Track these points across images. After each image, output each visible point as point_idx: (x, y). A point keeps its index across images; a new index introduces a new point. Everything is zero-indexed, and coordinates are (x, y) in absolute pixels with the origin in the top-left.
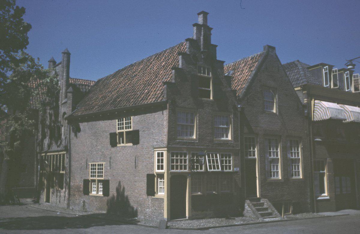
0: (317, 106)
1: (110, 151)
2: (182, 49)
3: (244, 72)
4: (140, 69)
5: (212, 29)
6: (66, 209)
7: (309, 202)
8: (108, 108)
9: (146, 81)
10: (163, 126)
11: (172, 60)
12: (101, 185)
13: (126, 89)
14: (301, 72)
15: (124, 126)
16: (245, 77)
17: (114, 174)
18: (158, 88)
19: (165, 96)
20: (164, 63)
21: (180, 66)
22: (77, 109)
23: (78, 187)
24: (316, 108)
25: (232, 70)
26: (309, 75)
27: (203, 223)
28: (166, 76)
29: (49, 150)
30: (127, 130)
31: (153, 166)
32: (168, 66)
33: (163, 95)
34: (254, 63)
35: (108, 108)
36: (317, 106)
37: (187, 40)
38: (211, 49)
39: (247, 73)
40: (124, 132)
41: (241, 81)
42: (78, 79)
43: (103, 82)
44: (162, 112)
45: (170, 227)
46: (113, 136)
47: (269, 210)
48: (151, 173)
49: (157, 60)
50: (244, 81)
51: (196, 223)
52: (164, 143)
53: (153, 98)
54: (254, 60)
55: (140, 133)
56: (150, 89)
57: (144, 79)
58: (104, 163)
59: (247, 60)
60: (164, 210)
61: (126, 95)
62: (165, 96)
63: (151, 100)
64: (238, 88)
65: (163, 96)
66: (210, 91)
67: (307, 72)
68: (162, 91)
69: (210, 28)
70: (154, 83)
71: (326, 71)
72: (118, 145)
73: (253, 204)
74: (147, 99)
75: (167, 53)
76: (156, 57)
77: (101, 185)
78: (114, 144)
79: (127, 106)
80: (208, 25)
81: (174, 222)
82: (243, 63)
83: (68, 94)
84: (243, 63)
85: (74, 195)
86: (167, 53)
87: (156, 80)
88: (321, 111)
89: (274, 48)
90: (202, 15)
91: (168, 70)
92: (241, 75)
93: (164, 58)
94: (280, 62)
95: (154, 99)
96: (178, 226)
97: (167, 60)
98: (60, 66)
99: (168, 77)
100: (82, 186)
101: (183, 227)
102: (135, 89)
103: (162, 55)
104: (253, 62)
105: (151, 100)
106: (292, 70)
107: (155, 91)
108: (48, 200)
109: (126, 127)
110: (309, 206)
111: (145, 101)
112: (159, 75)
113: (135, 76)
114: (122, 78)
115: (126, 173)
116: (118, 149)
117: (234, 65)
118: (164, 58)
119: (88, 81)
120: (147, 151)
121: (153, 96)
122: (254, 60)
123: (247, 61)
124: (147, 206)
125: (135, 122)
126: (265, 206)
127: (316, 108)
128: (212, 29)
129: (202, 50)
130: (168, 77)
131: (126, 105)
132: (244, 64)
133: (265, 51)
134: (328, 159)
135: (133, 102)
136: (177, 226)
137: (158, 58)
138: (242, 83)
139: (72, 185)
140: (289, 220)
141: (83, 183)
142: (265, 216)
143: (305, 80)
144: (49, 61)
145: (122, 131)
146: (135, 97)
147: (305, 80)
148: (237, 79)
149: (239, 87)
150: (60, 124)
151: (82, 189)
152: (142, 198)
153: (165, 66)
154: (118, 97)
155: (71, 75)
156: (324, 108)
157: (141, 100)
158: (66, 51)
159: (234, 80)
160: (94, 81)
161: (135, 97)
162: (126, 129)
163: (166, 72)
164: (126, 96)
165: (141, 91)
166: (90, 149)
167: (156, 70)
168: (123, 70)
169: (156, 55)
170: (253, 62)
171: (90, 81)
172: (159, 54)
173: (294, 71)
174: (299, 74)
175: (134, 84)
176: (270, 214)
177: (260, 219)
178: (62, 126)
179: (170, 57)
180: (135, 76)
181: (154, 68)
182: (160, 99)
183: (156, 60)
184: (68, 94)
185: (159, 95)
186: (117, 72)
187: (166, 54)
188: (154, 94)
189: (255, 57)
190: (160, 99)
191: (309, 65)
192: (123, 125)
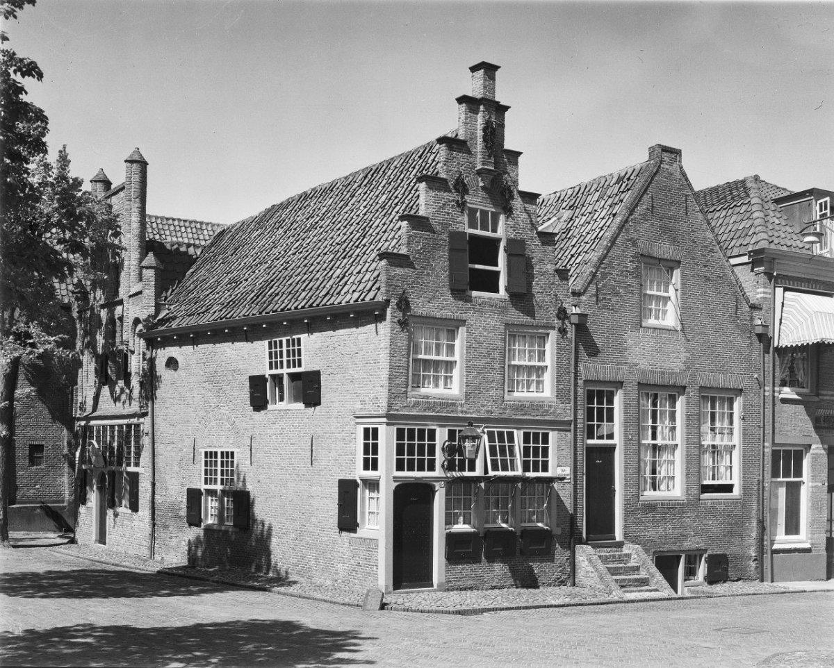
0: (791, 306)
1: (251, 422)
2: (430, 162)
3: (595, 218)
4: (325, 209)
5: (507, 108)
6: (146, 561)
7: (753, 554)
8: (241, 312)
9: (338, 244)
10: (378, 363)
11: (405, 191)
12: (230, 502)
13: (288, 263)
14: (756, 215)
15: (285, 359)
16: (598, 230)
17: (261, 478)
18: (367, 265)
19: (383, 289)
20: (385, 196)
21: (422, 213)
22: (168, 312)
23: (173, 509)
24: (789, 313)
25: (568, 208)
26: (777, 222)
27: (472, 599)
28: (386, 234)
29: (95, 414)
30: (292, 370)
31: (353, 461)
32: (393, 206)
33: (377, 286)
34: (623, 192)
35: (243, 312)
36: (791, 306)
37: (441, 140)
38: (503, 160)
39: (604, 221)
40: (285, 375)
41: (587, 243)
42: (168, 219)
43: (233, 237)
44: (374, 325)
45: (390, 607)
46: (257, 384)
47: (642, 573)
48: (349, 477)
49: (368, 185)
50: (594, 242)
51: (454, 599)
52: (379, 406)
53: (354, 291)
54: (624, 185)
55: (323, 378)
56: (348, 267)
57: (335, 237)
58: (236, 450)
59: (607, 183)
60: (379, 567)
61: (287, 278)
62: (383, 289)
63: (349, 296)
64: (577, 261)
65: (379, 289)
66: (498, 273)
67: (772, 214)
68: (376, 273)
69: (501, 105)
70: (359, 250)
71: (824, 212)
72: (270, 407)
73: (600, 557)
74: (339, 293)
75: (392, 167)
76: (365, 177)
77: (230, 502)
78: (259, 403)
79: (290, 309)
80: (497, 99)
81: (402, 595)
82: (596, 190)
83: (144, 271)
84: (596, 190)
85: (166, 527)
86: (392, 167)
87: (363, 243)
88: (798, 320)
89: (676, 153)
90: (481, 72)
91: (393, 219)
92: (589, 223)
93: (385, 182)
94: (690, 185)
95: (356, 295)
96: (410, 604)
97: (393, 191)
98: (122, 194)
99: (393, 238)
100: (184, 505)
101: (421, 608)
102: (312, 265)
103: (381, 172)
104: (621, 190)
105: (348, 297)
106: (732, 206)
107: (359, 273)
108: (102, 539)
109: (288, 362)
110: (753, 564)
111: (333, 298)
112: (371, 230)
113: (313, 227)
114: (281, 231)
115: (288, 477)
116: (270, 416)
117: (574, 194)
118: (385, 182)
119: (195, 222)
120: (339, 425)
121: (354, 287)
122: (624, 185)
123: (605, 187)
124: (339, 557)
125: (314, 349)
126: (632, 563)
127: (789, 313)
128: (507, 108)
129: (479, 167)
130: (393, 238)
131: (289, 307)
132: (598, 194)
133: (652, 162)
134: (814, 446)
135: (304, 299)
136: (407, 605)
137: (370, 182)
138: (588, 245)
139: (160, 501)
140: (695, 598)
141: (185, 497)
142: (630, 586)
143: (764, 236)
144: (91, 181)
145: (279, 371)
146: (309, 287)
147: (764, 236)
148: (578, 236)
149: (580, 258)
150: (126, 349)
151: (183, 513)
152: (327, 537)
153: (386, 207)
154: (269, 284)
155: (149, 211)
156: (807, 312)
157: (325, 296)
158: (136, 157)
159: (569, 238)
160: (211, 223)
161: (309, 287)
162: (289, 366)
163: (387, 222)
164: (289, 282)
165: (325, 269)
166: (202, 413)
167: (365, 214)
168: (283, 206)
169: (366, 171)
170: (621, 190)
171: (201, 223)
172: (374, 168)
173: (737, 209)
174: (748, 218)
175: (310, 251)
176: (644, 582)
177: (614, 593)
178: (133, 352)
179: (399, 181)
180: (313, 227)
181: (359, 209)
182: (371, 295)
183: (365, 186)
184: (144, 271)
185: (370, 284)
186: (268, 211)
187: (390, 171)
188: (356, 282)
189: (627, 176)
190: (371, 295)
191: (785, 189)
192: (288, 351)
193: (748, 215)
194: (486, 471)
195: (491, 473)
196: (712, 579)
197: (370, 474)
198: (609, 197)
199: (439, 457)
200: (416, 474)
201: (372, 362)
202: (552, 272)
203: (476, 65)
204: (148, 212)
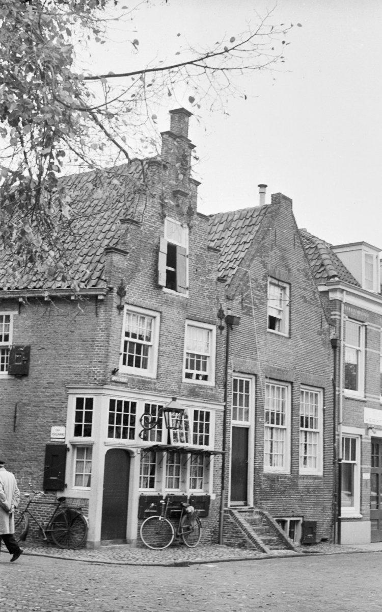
193: (316, 256)
194: (169, 442)
195: (173, 444)
196: (305, 542)
197: (82, 440)
198: (235, 229)
199: (139, 428)
200: (121, 441)
201: (90, 340)
202: (215, 280)
203: (178, 109)
204: (146, 73)
